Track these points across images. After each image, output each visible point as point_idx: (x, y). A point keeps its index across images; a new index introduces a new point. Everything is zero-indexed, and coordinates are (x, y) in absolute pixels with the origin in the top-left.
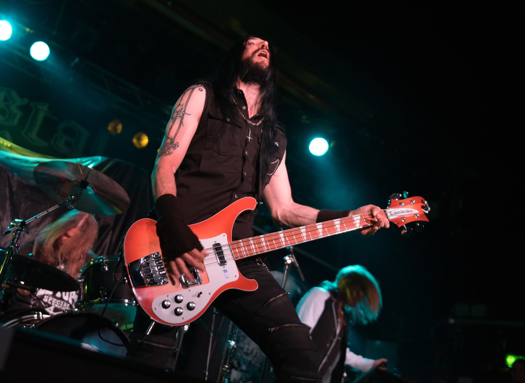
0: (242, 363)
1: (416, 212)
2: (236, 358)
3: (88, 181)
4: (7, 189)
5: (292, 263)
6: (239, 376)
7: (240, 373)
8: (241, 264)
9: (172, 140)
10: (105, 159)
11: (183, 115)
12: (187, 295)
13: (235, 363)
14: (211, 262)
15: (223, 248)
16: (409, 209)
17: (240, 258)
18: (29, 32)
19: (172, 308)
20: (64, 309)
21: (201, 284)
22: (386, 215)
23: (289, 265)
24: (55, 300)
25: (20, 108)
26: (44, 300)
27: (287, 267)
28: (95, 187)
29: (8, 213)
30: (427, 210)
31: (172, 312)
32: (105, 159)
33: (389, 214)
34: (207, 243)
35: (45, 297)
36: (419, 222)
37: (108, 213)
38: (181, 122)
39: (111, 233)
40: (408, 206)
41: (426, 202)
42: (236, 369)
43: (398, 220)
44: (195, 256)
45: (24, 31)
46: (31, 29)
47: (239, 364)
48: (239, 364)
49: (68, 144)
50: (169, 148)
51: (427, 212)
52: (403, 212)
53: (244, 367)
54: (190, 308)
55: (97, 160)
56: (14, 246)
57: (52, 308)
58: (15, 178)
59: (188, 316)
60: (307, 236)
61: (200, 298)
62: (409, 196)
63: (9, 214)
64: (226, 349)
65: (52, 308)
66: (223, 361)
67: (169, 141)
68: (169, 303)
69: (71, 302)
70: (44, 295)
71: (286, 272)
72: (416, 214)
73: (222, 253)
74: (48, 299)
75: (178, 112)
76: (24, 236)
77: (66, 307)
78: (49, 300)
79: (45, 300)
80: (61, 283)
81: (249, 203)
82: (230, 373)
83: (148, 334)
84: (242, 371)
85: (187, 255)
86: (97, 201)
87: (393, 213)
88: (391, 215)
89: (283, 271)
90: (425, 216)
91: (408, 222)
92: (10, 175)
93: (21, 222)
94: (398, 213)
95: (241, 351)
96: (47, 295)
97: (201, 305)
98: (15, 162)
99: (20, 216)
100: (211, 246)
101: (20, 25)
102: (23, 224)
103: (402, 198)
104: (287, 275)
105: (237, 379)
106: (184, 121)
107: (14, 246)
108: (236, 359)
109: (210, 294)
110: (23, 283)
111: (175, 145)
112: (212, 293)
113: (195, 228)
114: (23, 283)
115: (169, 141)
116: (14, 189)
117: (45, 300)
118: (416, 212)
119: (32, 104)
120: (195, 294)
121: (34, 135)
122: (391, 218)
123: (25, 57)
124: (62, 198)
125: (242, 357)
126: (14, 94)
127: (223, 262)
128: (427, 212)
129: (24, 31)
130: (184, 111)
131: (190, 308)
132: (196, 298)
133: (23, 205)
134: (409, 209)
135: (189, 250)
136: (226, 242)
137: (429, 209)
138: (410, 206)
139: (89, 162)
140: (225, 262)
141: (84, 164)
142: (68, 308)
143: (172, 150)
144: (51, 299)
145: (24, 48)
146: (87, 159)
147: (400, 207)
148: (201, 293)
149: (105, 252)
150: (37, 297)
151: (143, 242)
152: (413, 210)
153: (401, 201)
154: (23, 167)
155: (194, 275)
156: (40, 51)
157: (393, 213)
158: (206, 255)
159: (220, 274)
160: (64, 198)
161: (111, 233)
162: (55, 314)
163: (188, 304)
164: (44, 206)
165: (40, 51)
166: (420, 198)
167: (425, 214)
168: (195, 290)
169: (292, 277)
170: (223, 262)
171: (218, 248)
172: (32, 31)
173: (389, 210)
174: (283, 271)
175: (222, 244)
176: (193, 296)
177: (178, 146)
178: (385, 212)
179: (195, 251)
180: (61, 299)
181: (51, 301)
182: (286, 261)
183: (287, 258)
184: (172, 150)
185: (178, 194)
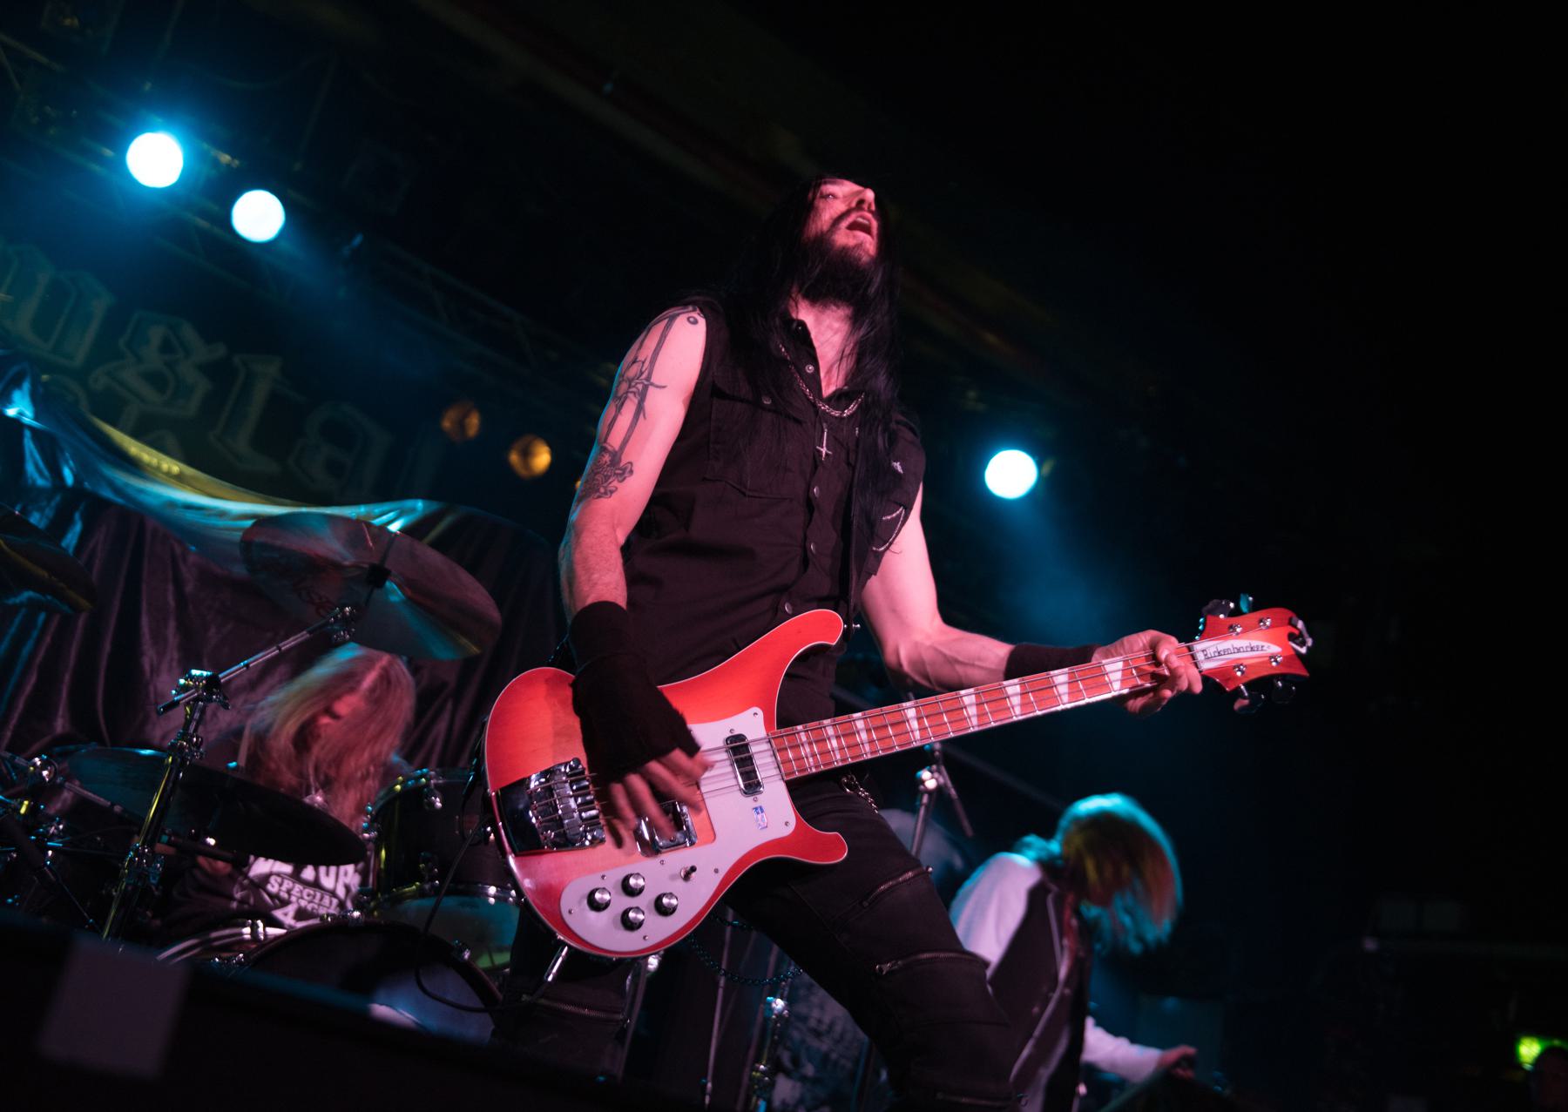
0: (804, 1059)
4: (171, 587)
6: (797, 1094)
7: (799, 1085)
8: (800, 789)
9: (616, 457)
10: (434, 506)
11: (646, 388)
12: (654, 874)
13: (786, 1058)
14: (719, 789)
15: (753, 749)
16: (1260, 643)
17: (797, 774)
18: (228, 165)
20: (322, 911)
22: (1193, 657)
24: (298, 887)
25: (208, 369)
26: (269, 887)
27: (925, 799)
28: (407, 584)
29: (173, 654)
30: (1303, 644)
32: (434, 506)
33: (1200, 657)
34: (710, 734)
35: (272, 879)
36: (1282, 677)
38: (640, 409)
39: (449, 706)
40: (1250, 634)
41: (1300, 624)
42: (788, 1074)
44: (676, 770)
46: (233, 157)
47: (796, 1061)
48: (796, 1061)
50: (607, 478)
51: (1303, 650)
54: (663, 910)
56: (189, 741)
57: (291, 909)
58: (191, 559)
59: (659, 930)
60: (979, 716)
61: (690, 883)
62: (1254, 608)
63: (176, 655)
64: (760, 1019)
65: (291, 909)
66: (752, 1053)
67: (607, 458)
68: (607, 897)
69: (341, 892)
70: (271, 874)
72: (1273, 657)
75: (630, 381)
76: (214, 715)
77: (328, 908)
78: (284, 888)
79: (273, 887)
80: (315, 842)
81: (820, 627)
82: (772, 1085)
84: (803, 1079)
85: (655, 767)
87: (1211, 652)
88: (1208, 659)
90: (1298, 661)
91: (1253, 677)
92: (178, 550)
94: (1226, 652)
95: (799, 1025)
96: (278, 875)
97: (692, 901)
98: (190, 516)
100: (721, 743)
101: (206, 146)
102: (212, 682)
103: (1237, 612)
104: (926, 822)
106: (648, 404)
109: (716, 871)
110: (212, 841)
111: (624, 470)
112: (724, 869)
113: (678, 695)
114: (212, 841)
115: (607, 458)
122: (1206, 666)
123: (217, 231)
125: (803, 1041)
126: (189, 332)
127: (752, 785)
130: (648, 378)
131: (663, 910)
133: (213, 630)
134: (1255, 643)
135: (660, 754)
137: (1310, 642)
138: (1259, 634)
139: (391, 515)
140: (759, 784)
141: (377, 522)
143: (615, 483)
144: (287, 884)
146: (386, 506)
148: (693, 869)
149: (435, 758)
150: (251, 881)
151: (539, 734)
153: (1233, 620)
156: (259, 216)
157: (1211, 652)
158: (707, 767)
159: (746, 819)
161: (449, 706)
162: (300, 925)
163: (659, 898)
164: (269, 635)
166: (1284, 613)
167: (1298, 654)
168: (677, 860)
170: (752, 785)
171: (738, 748)
172: (237, 162)
173: (1200, 646)
175: (749, 738)
176: (673, 878)
177: (631, 472)
178: (1190, 649)
179: (678, 756)
181: (289, 892)
182: (923, 782)
184: (615, 483)
185: (629, 603)
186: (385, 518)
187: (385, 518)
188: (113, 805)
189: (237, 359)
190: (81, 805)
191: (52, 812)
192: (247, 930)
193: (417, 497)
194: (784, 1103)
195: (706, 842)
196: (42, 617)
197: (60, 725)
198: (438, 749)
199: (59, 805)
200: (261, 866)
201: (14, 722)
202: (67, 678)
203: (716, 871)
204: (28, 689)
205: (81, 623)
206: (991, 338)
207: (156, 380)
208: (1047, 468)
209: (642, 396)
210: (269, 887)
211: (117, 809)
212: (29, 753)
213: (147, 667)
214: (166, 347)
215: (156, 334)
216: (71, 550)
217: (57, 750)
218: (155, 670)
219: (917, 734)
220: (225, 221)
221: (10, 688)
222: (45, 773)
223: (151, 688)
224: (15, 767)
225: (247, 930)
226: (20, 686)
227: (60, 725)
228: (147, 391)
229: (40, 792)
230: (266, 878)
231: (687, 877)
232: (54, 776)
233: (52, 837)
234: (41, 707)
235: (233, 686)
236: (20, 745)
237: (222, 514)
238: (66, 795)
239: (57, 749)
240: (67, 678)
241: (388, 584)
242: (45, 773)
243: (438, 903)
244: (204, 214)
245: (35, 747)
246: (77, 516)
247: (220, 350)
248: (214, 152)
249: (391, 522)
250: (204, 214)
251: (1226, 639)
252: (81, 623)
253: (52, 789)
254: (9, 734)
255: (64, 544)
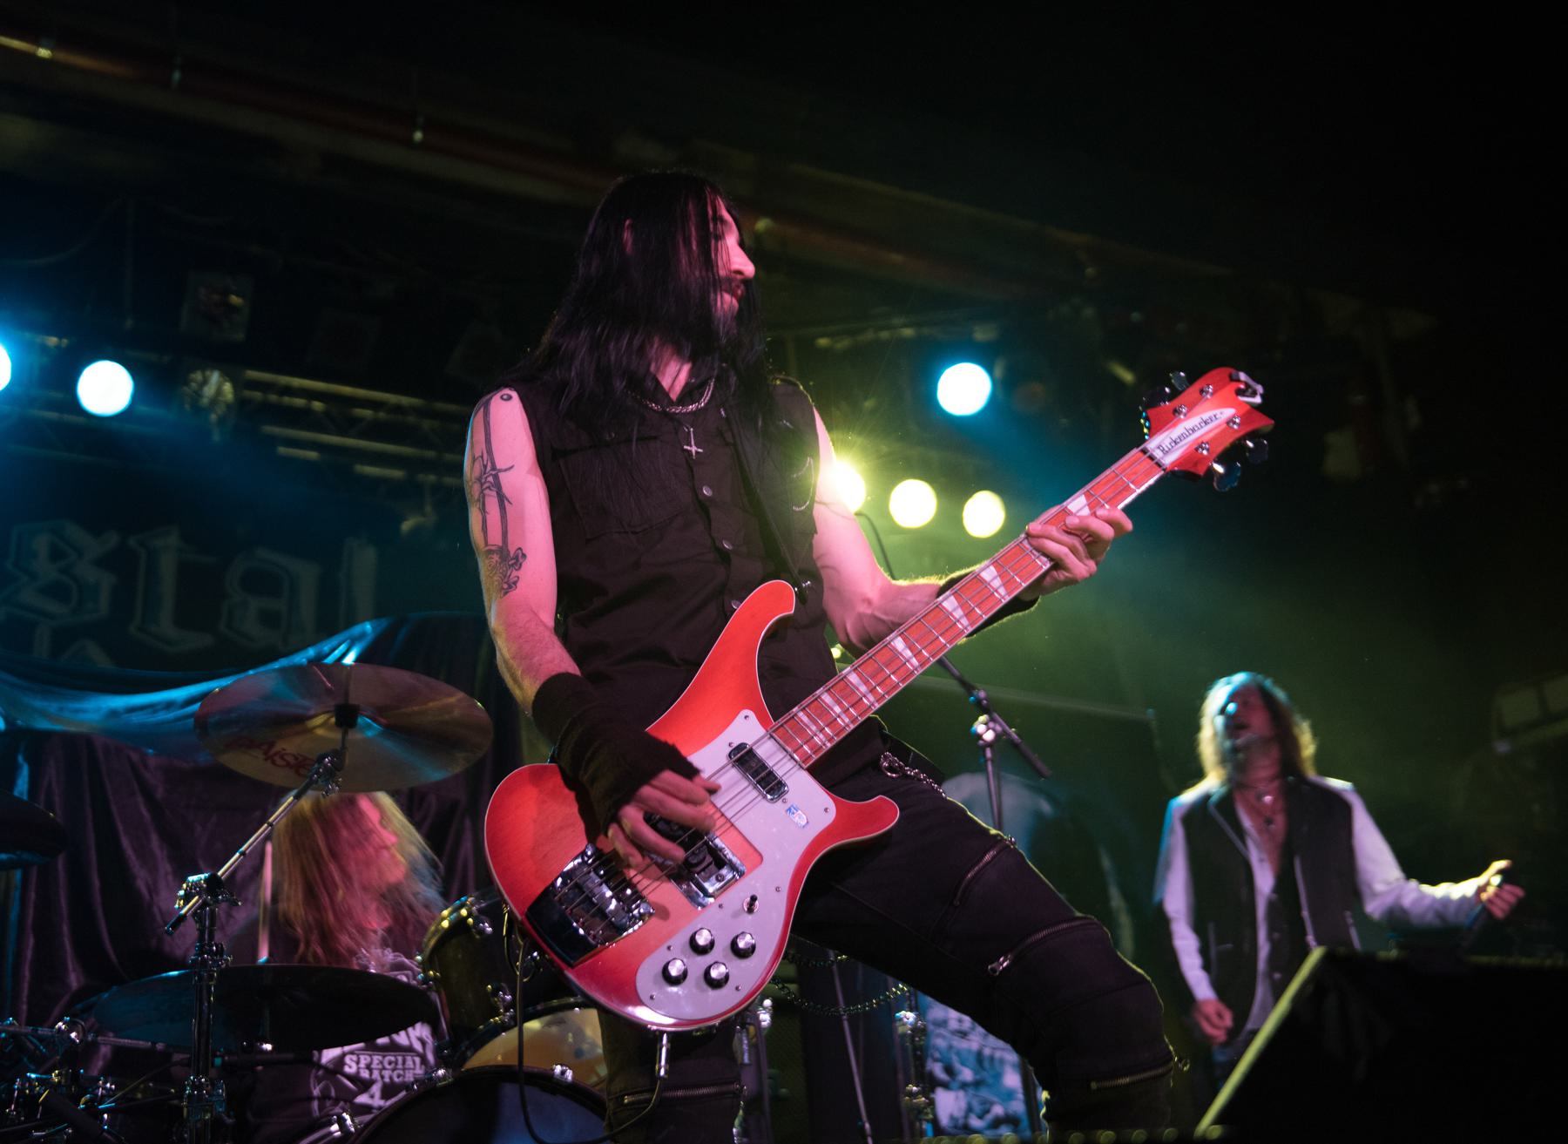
0: (957, 1066)
1: (1229, 412)
2: (937, 1055)
3: (353, 701)
4: (140, 799)
5: (998, 736)
6: (963, 1105)
7: (961, 1094)
8: (826, 771)
10: (384, 623)
11: (496, 477)
13: (938, 1070)
16: (1211, 413)
17: (815, 757)
18: (58, 347)
19: (696, 974)
20: (409, 1077)
21: (742, 874)
22: (1152, 458)
23: (990, 745)
24: (377, 1058)
25: (103, 563)
26: (347, 1069)
27: (989, 753)
28: (379, 713)
29: (165, 867)
30: (1254, 394)
31: (698, 986)
32: (384, 623)
33: (1158, 454)
35: (347, 1059)
36: (1251, 435)
37: (433, 773)
38: (502, 499)
39: (468, 823)
40: (1199, 408)
42: (946, 1086)
43: (1192, 456)
45: (44, 349)
46: (60, 338)
47: (949, 1070)
48: (949, 1070)
49: (269, 619)
51: (1258, 400)
52: (1193, 430)
53: (967, 1074)
55: (363, 636)
56: (210, 952)
57: (376, 1089)
58: (152, 762)
59: (749, 975)
63: (168, 867)
65: (376, 1089)
66: (901, 1076)
68: (722, 969)
69: (418, 1046)
70: (344, 1055)
71: (990, 768)
72: (1230, 421)
73: (762, 766)
74: (358, 1063)
76: (229, 915)
77: (413, 1070)
78: (362, 1065)
79: (350, 1068)
80: (373, 1010)
83: (662, 1072)
84: (964, 1086)
86: (391, 747)
88: (1166, 453)
89: (984, 770)
90: (1257, 415)
92: (135, 757)
93: (206, 880)
95: (942, 1031)
96: (352, 1053)
97: (767, 929)
98: (136, 718)
99: (202, 864)
100: (724, 760)
101: (28, 335)
102: (213, 881)
104: (998, 778)
105: (959, 1114)
106: (505, 490)
107: (210, 952)
108: (936, 1060)
110: (268, 1047)
112: (785, 882)
114: (268, 1047)
116: (160, 794)
117: (350, 1068)
118: (1229, 412)
119: (132, 542)
120: (738, 906)
121: (165, 624)
122: (1168, 461)
123: (68, 418)
124: (298, 773)
125: (950, 1047)
126: (74, 532)
127: (770, 784)
128: (1258, 400)
129: (44, 349)
132: (750, 917)
133: (199, 829)
134: (1206, 416)
135: (648, 776)
136: (760, 731)
137: (1260, 389)
138: (1207, 404)
139: (343, 648)
141: (330, 660)
142: (419, 1071)
144: (364, 1060)
145: (57, 395)
146: (334, 641)
147: (1180, 421)
148: (754, 899)
149: (471, 883)
150: (325, 1068)
152: (1217, 412)
153: (1176, 402)
154: (164, 723)
155: (696, 855)
156: (106, 388)
159: (782, 827)
160: (303, 771)
161: (468, 823)
162: (389, 1103)
163: (734, 944)
164: (258, 813)
165: (106, 388)
169: (1013, 777)
170: (770, 784)
171: (744, 758)
172: (65, 341)
173: (1152, 445)
174: (984, 770)
175: (749, 742)
176: (736, 915)
177: (524, 556)
178: (1144, 451)
179: (669, 777)
180: (394, 1048)
181: (368, 1067)
182: (979, 737)
183: (979, 727)
184: (515, 573)
186: (337, 653)
187: (337, 653)
188: (154, 1043)
189: (132, 542)
190: (118, 1051)
191: (95, 1073)
192: (335, 1127)
193: (363, 621)
194: (952, 1118)
195: (755, 866)
196: (18, 875)
197: (74, 980)
198: (471, 873)
199: (100, 1064)
200: (329, 1055)
201: (26, 992)
202: (65, 928)
203: (777, 889)
204: (29, 954)
205: (60, 866)
206: (897, 258)
207: (55, 591)
208: (998, 372)
209: (497, 485)
210: (347, 1069)
211: (160, 1046)
212: (52, 1020)
213: (144, 891)
214: (56, 555)
215: (41, 544)
216: (25, 798)
217: (78, 1008)
218: (153, 890)
219: (914, 661)
220: (74, 405)
221: (10, 959)
222: (73, 1035)
223: (156, 910)
224: (42, 1039)
225: (335, 1127)
226: (19, 954)
227: (74, 980)
228: (52, 607)
229: (75, 1057)
230: (340, 1061)
231: (750, 910)
232: (83, 1033)
233: (102, 1100)
234: (48, 967)
235: (240, 874)
236: (40, 1016)
237: (169, 705)
238: (105, 1050)
239: (79, 1006)
240: (65, 928)
241: (360, 720)
242: (73, 1035)
243: (521, 1031)
244: (51, 405)
245: (56, 1012)
246: (20, 759)
247: (113, 539)
248: (39, 339)
249: (344, 655)
250: (51, 405)
251: (1175, 425)
252: (60, 866)
253: (87, 1050)
254: (25, 1007)
255: (16, 793)
